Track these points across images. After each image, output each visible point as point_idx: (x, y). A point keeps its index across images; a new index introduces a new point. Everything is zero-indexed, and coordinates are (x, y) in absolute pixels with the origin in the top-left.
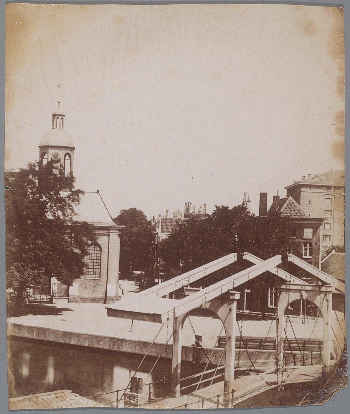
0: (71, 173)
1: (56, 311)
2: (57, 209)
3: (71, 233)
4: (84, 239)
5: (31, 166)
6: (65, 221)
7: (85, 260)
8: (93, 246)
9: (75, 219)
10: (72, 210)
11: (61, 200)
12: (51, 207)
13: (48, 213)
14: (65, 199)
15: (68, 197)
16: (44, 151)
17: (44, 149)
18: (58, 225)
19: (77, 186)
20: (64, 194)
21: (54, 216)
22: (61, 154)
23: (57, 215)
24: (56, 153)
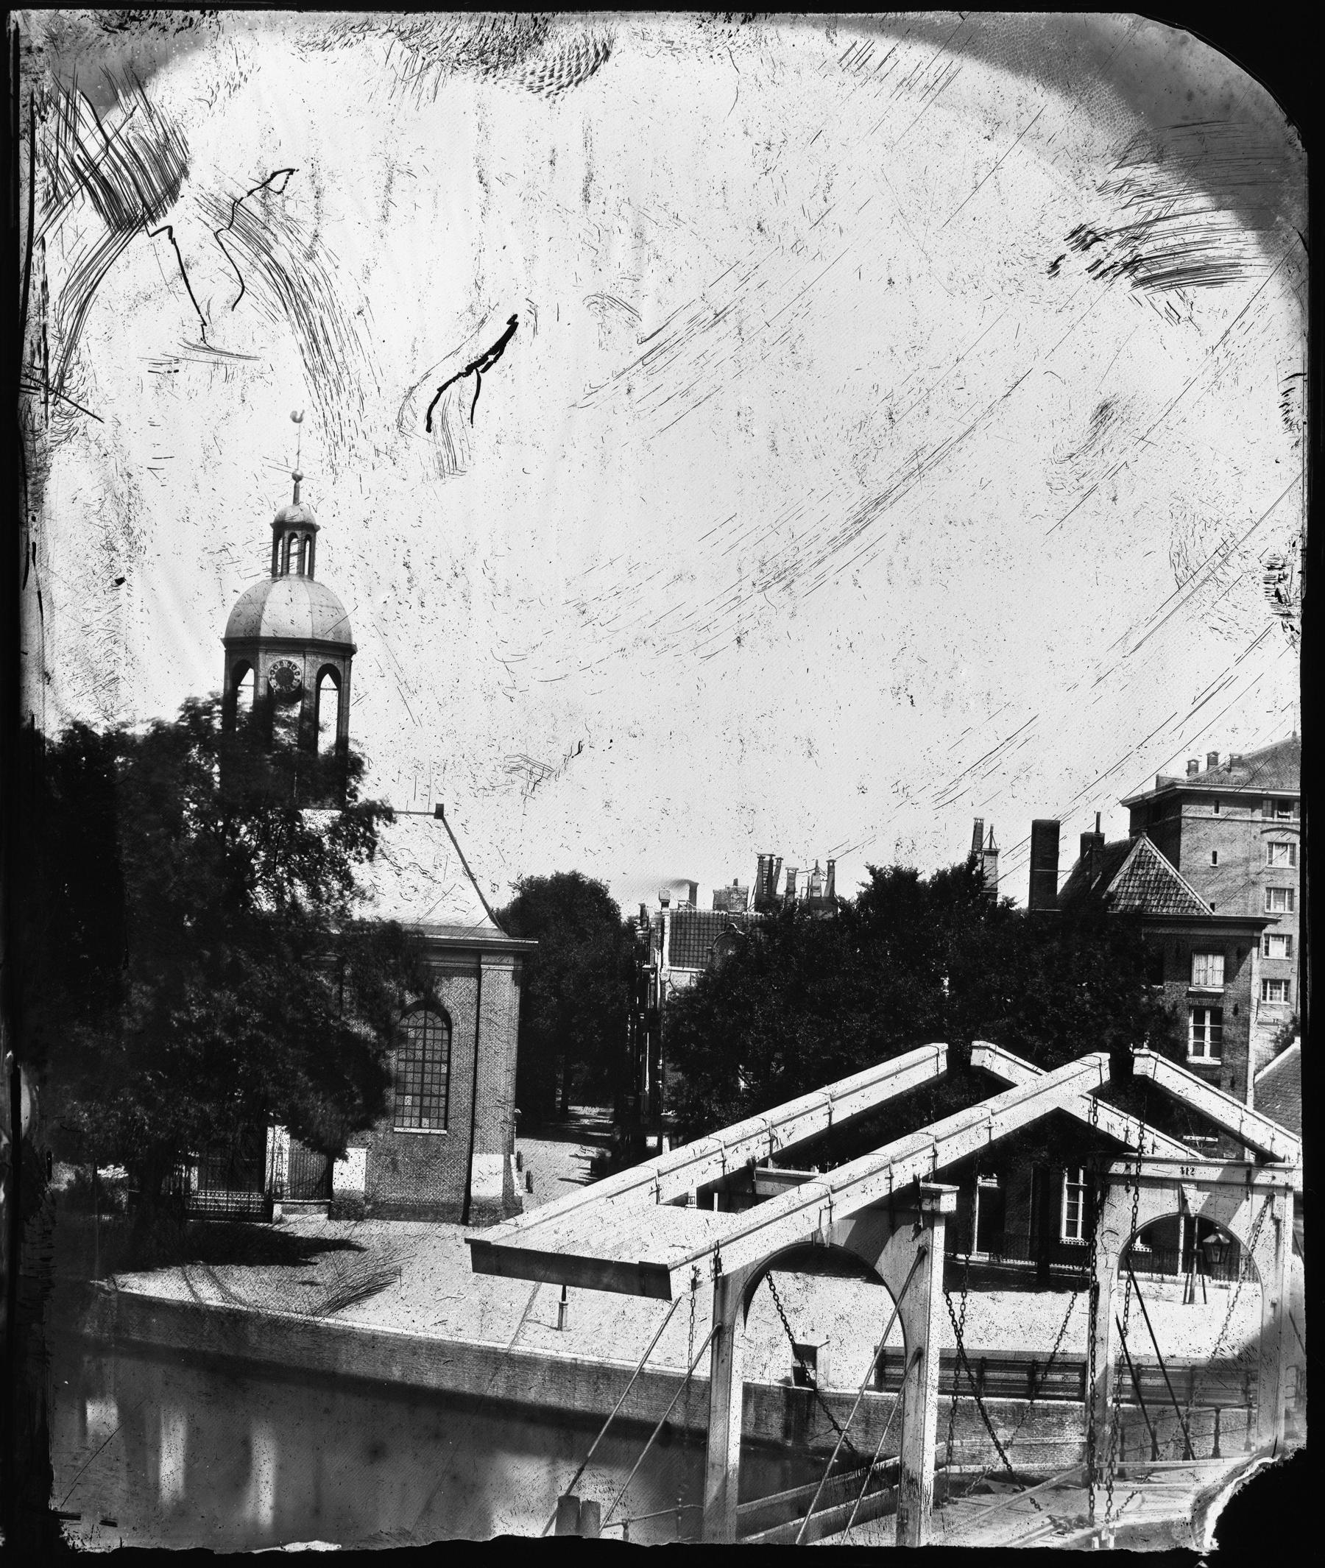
0: (342, 741)
1: (295, 1252)
2: (292, 873)
3: (342, 962)
4: (391, 985)
5: (193, 710)
6: (318, 919)
7: (394, 1060)
8: (421, 1014)
9: (360, 911)
10: (347, 880)
11: (310, 842)
12: (268, 868)
13: (258, 889)
14: (319, 839)
15: (334, 831)
16: (240, 658)
17: (243, 648)
18: (297, 933)
19: (367, 791)
20: (318, 819)
21: (280, 900)
22: (304, 667)
23: (287, 898)
24: (285, 665)
